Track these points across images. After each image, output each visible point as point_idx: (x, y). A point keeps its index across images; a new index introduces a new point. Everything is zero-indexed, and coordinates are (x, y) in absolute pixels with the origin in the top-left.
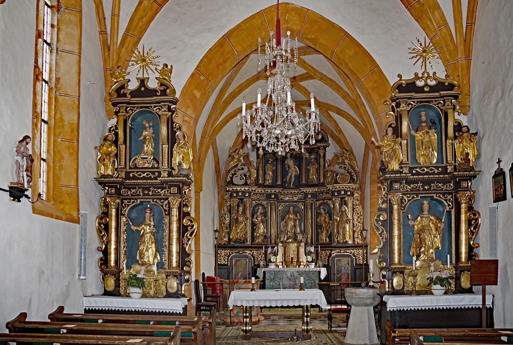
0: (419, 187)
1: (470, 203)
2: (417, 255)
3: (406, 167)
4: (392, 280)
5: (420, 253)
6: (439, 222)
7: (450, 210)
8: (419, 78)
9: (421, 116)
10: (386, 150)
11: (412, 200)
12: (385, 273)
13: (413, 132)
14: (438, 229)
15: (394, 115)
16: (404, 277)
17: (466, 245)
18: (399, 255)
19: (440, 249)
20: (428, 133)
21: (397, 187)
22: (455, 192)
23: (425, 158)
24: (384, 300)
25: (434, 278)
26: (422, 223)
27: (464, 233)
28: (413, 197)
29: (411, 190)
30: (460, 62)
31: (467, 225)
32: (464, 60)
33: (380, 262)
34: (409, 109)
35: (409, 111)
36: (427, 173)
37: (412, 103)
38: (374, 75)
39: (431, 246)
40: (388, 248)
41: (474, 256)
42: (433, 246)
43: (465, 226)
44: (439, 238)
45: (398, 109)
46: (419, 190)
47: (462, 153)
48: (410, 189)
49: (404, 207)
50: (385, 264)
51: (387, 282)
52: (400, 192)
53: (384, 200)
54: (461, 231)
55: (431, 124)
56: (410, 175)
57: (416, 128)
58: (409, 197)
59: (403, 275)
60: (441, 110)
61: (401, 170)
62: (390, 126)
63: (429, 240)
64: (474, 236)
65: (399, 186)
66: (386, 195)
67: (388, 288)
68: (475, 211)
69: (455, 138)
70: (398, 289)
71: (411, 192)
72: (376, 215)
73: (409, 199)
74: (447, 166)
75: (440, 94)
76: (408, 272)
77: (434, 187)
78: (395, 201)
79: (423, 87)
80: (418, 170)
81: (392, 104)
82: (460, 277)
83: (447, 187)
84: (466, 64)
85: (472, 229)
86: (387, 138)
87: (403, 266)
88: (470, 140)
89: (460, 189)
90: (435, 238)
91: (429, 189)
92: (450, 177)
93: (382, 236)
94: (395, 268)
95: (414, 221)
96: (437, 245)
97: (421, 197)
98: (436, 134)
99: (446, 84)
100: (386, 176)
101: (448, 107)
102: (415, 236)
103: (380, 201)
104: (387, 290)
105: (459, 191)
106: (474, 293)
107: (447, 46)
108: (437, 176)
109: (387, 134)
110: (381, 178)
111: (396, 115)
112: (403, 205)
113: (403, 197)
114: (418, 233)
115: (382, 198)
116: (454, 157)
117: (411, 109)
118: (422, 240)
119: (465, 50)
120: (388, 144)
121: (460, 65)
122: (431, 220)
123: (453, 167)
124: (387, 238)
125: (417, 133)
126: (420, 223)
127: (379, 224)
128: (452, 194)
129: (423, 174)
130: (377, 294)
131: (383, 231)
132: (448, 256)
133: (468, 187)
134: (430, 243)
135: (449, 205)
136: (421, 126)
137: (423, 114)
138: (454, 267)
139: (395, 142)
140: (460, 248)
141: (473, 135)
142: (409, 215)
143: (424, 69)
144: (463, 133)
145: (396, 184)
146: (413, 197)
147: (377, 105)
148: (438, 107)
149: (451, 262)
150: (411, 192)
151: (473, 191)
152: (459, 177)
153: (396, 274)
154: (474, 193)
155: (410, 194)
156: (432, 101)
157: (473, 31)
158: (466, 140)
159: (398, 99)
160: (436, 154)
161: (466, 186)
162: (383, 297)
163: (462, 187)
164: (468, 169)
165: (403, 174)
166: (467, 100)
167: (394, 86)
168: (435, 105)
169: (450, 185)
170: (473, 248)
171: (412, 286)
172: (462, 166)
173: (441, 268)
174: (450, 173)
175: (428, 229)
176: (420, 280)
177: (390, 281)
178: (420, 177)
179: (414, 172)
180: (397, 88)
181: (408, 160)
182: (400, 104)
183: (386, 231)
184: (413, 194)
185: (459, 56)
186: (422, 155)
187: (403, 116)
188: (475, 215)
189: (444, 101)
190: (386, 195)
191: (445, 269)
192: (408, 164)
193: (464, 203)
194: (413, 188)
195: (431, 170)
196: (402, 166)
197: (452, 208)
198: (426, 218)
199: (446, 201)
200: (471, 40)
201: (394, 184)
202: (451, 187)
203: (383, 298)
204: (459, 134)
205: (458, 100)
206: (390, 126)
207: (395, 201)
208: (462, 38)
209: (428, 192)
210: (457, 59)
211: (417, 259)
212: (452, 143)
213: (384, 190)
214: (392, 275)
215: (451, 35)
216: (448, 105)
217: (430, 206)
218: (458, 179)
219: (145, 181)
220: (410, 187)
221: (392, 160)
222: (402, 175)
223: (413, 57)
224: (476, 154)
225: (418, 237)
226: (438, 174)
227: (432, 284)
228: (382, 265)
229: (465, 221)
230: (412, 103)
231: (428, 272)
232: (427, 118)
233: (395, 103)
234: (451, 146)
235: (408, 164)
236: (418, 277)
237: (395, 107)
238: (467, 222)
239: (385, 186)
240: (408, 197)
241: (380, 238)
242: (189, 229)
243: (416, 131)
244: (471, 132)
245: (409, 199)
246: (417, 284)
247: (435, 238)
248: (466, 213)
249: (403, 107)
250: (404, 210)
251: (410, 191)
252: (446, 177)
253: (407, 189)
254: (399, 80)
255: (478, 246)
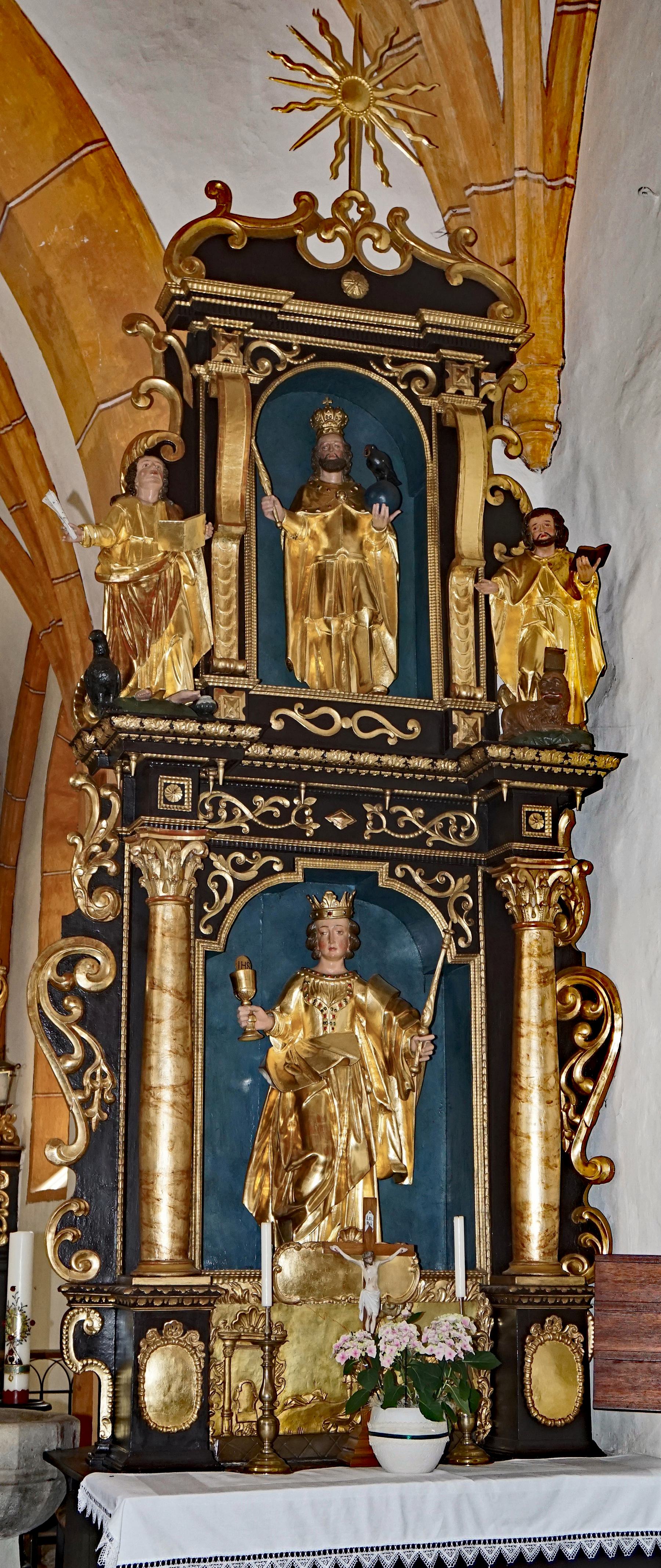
0: (301, 817)
1: (565, 926)
2: (284, 1211)
3: (230, 690)
4: (138, 1370)
5: (301, 1200)
6: (403, 1024)
7: (463, 959)
8: (317, 225)
9: (318, 433)
10: (125, 577)
11: (258, 888)
12: (93, 1322)
13: (272, 507)
14: (401, 1061)
15: (177, 398)
16: (209, 1352)
17: (546, 1162)
18: (184, 1213)
19: (407, 1181)
20: (351, 524)
21: (178, 797)
22: (490, 863)
23: (335, 657)
24: (83, 1501)
25: (386, 1362)
26: (313, 1020)
27: (535, 1096)
28: (267, 871)
29: (256, 831)
30: (520, 186)
31: (552, 1050)
32: (541, 187)
33: (65, 1252)
34: (255, 380)
35: (256, 391)
36: (345, 741)
37: (273, 347)
38: (77, 181)
39: (360, 1160)
40: (113, 1165)
41: (590, 1227)
42: (372, 1163)
43: (544, 1054)
44: (400, 1115)
45: (200, 369)
46: (300, 834)
47: (524, 654)
48: (250, 823)
49: (217, 922)
50: (95, 1263)
51: (105, 1379)
52: (199, 830)
53: (103, 870)
54: (524, 1083)
55: (369, 479)
56: (253, 732)
57: (291, 494)
58: (246, 867)
59: (205, 1338)
60: (425, 412)
61: (206, 700)
62: (154, 451)
63: (351, 1127)
64: (587, 1117)
65: (189, 795)
66: (114, 844)
67: (114, 1419)
68: (591, 973)
69: (492, 569)
70: (172, 1427)
71: (255, 841)
72: (56, 959)
73: (241, 876)
74: (447, 714)
75: (424, 326)
76: (230, 1320)
77: (377, 823)
78: (163, 877)
79: (336, 274)
80: (295, 715)
81: (170, 338)
82: (524, 1354)
83: (444, 831)
84: (546, 208)
85: (578, 1073)
86: (133, 512)
87: (205, 1281)
88: (569, 585)
89: (517, 845)
90: (382, 1119)
91: (353, 833)
92: (466, 773)
93: (82, 1088)
94: (155, 1291)
95: (268, 1008)
96: (392, 1155)
97: (306, 871)
98: (391, 540)
99: (457, 281)
100: (117, 721)
101: (459, 402)
102: (274, 1096)
103: (81, 874)
104: (106, 1431)
105: (509, 853)
106: (601, 1454)
107: (459, 99)
108: (399, 762)
109: (131, 490)
110: (90, 739)
111: (190, 400)
112: (211, 913)
113: (206, 861)
114: (291, 1084)
115: (90, 857)
116: (483, 666)
117: (266, 382)
118: (312, 1123)
119: (546, 138)
120: (136, 548)
121: (519, 206)
122: (359, 1008)
123: (478, 718)
124: (115, 1102)
125: (294, 519)
126: (297, 1024)
127: (68, 1012)
128: (470, 868)
129: (325, 744)
130: (47, 1456)
131: (88, 1059)
132: (459, 1223)
133: (554, 840)
134: (353, 1142)
135: (458, 932)
136: (316, 485)
137: (330, 420)
138: (489, 1294)
139: (175, 538)
140: (520, 1182)
141: (585, 560)
142: (241, 974)
143: (342, 185)
144: (534, 545)
145: (173, 780)
146: (267, 871)
147: (85, 353)
148: (408, 393)
149: (470, 1264)
150: (255, 841)
151: (580, 863)
152: (512, 774)
153: (160, 1329)
154: (583, 874)
155: (248, 850)
156: (379, 361)
157: (586, 40)
158: (548, 587)
159: (202, 311)
160: (390, 642)
161: (548, 832)
162: (77, 1486)
163: (527, 834)
164: (558, 734)
165: (213, 721)
166: (549, 393)
167: (186, 237)
168: (393, 380)
169: (461, 822)
170: (584, 1184)
171: (253, 1407)
172: (526, 720)
173: (413, 1299)
174: (468, 751)
175: (347, 1061)
176: (298, 1371)
177: (126, 1375)
178: (304, 753)
179: (276, 725)
180: (197, 254)
181: (242, 656)
182: (214, 344)
183: (111, 1059)
184: (265, 851)
185: (520, 159)
186: (316, 643)
187: (225, 406)
188: (589, 995)
189: (440, 369)
190: (114, 844)
191: (440, 1307)
192: (244, 674)
193: (537, 925)
194: (267, 817)
195: (367, 724)
196: (212, 680)
197: (473, 949)
198: (334, 995)
199: (441, 904)
200: (579, 88)
201: (163, 780)
202: (469, 833)
203: (81, 1495)
204: (508, 553)
205: (505, 379)
206: (154, 451)
207: (163, 877)
208: (535, 71)
209: (346, 846)
210: (505, 175)
211: (283, 1239)
212: (476, 593)
213: (105, 813)
214: (140, 1335)
215: (481, 49)
216: (460, 393)
217: (355, 931)
218: (509, 789)
219: (343, 756)
220: (252, 808)
221: (157, 635)
222: (209, 728)
223: (288, 108)
224: (598, 663)
225: (290, 1104)
226: (403, 749)
227: (374, 1402)
228: (77, 1274)
229: (544, 1025)
230: (273, 347)
231: (341, 1319)
232: (347, 447)
233: (183, 335)
234: (471, 609)
235: (244, 674)
236: (289, 1354)
237: (182, 355)
238: (551, 1029)
239: (113, 787)
240: (237, 867)
241: (75, 1098)
242: (579, 1039)
243: (293, 506)
244: (573, 545)
245: (241, 876)
246: (285, 1393)
247: (382, 1119)
248: (544, 981)
249: (227, 361)
250: (213, 937)
251: (250, 834)
252: (445, 773)
253: (230, 817)
254: (213, 214)
255: (612, 1173)
